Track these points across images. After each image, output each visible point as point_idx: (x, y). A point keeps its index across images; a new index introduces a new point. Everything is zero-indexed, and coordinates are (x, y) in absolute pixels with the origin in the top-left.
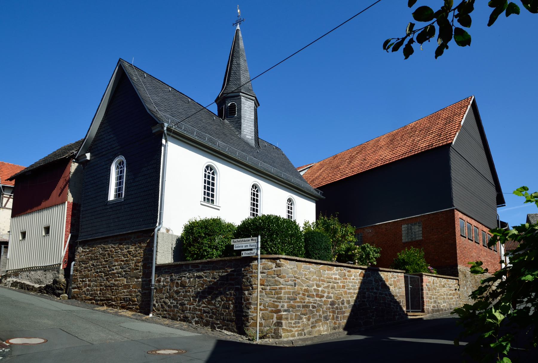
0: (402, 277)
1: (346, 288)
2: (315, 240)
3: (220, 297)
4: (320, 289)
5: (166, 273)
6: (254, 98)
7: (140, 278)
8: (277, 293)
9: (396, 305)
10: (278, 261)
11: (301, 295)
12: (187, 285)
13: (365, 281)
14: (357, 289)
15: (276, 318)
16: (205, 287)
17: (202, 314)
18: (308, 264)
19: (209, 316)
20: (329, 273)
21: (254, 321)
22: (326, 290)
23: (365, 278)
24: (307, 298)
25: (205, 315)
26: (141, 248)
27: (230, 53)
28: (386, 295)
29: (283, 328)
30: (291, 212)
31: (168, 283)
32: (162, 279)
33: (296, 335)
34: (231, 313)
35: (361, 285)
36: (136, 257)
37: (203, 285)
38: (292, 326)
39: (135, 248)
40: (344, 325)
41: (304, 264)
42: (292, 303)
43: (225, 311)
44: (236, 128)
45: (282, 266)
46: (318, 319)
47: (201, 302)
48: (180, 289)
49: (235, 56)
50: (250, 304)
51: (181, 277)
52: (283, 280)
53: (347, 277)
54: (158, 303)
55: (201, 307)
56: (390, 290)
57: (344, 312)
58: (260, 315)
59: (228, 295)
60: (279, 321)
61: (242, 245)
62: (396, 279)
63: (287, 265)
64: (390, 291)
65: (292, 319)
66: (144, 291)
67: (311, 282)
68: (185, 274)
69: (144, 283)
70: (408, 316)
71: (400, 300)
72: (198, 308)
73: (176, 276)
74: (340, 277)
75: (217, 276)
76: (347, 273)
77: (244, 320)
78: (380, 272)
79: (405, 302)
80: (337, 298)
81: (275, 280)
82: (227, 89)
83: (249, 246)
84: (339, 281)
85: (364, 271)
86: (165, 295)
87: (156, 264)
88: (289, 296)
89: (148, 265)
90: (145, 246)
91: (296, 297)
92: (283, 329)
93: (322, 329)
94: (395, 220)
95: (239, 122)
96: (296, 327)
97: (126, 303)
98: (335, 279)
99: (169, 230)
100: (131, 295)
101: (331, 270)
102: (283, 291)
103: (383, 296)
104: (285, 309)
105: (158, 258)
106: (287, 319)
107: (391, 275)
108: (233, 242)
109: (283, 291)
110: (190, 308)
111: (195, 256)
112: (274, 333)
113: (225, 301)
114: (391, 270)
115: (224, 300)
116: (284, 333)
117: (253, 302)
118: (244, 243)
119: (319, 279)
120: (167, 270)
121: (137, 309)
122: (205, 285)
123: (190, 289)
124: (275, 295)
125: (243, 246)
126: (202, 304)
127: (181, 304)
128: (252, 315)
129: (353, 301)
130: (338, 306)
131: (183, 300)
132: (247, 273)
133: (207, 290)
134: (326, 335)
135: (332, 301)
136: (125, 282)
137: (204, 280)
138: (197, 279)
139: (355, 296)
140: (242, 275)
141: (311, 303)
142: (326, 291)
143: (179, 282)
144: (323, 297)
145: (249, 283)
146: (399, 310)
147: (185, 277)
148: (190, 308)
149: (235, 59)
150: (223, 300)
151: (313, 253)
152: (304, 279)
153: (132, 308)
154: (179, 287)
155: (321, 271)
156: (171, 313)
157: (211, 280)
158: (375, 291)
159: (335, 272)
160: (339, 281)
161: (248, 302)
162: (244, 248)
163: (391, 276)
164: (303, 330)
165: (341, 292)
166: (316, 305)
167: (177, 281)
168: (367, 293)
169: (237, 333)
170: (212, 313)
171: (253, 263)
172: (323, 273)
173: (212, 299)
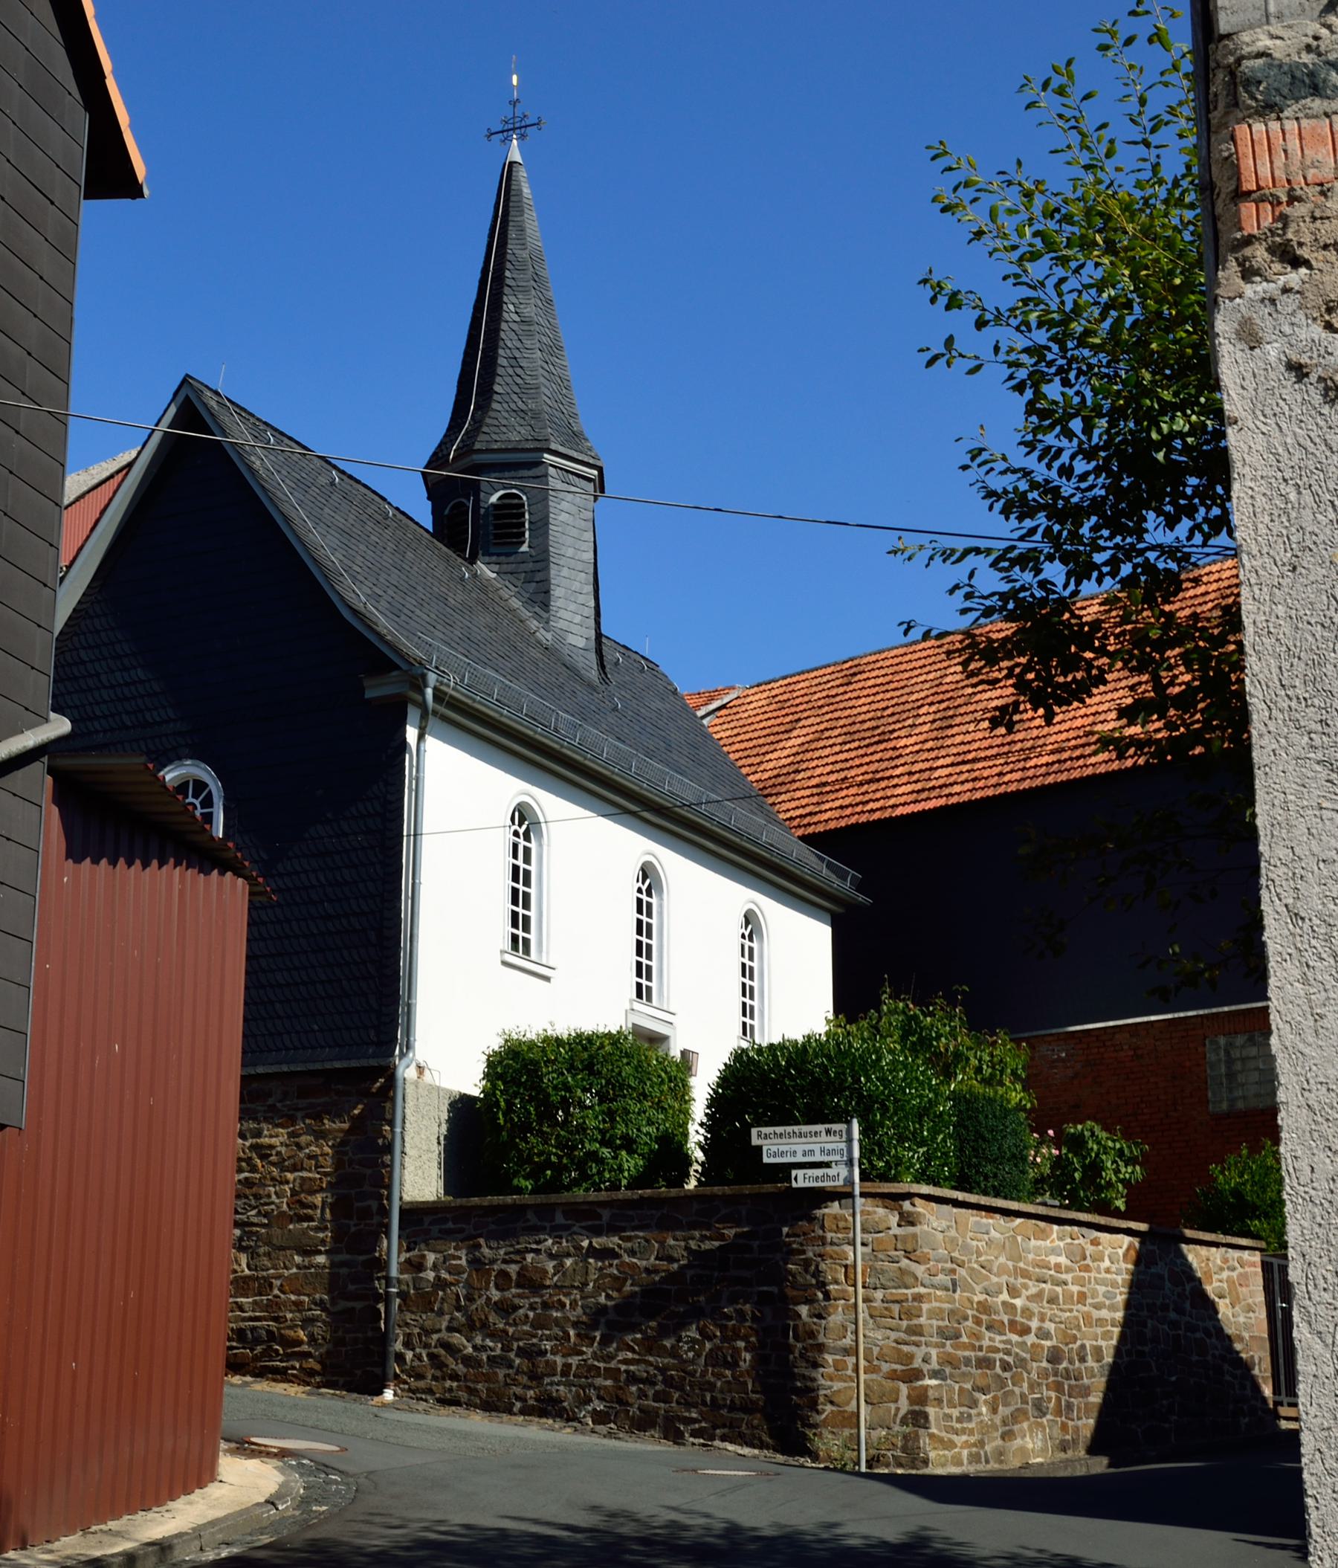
0: (1253, 1265)
1: (1089, 1301)
2: (980, 1123)
3: (694, 1327)
4: (1018, 1302)
5: (447, 1235)
6: (596, 472)
7: (319, 1252)
8: (909, 1314)
9: (1239, 1372)
10: (906, 1205)
11: (969, 1323)
12: (548, 1283)
13: (1141, 1277)
14: (1121, 1306)
15: (909, 1397)
16: (628, 1288)
17: (621, 1388)
18: (984, 1213)
19: (651, 1393)
20: (1039, 1248)
21: (834, 1408)
22: (1034, 1307)
23: (1142, 1267)
24: (988, 1334)
25: (634, 1389)
26: (320, 1135)
27: (480, 265)
28: (1209, 1335)
29: (930, 1431)
31: (459, 1273)
32: (431, 1257)
33: (965, 1461)
34: (745, 1383)
35: (1130, 1293)
36: (294, 1169)
37: (618, 1282)
38: (952, 1427)
39: (291, 1135)
40: (1089, 1435)
42: (951, 1350)
43: (719, 1376)
44: (530, 602)
45: (920, 1223)
46: (1017, 1410)
47: (615, 1345)
48: (519, 1296)
49: (508, 282)
50: (821, 1348)
51: (522, 1253)
52: (922, 1268)
53: (1088, 1261)
54: (413, 1350)
55: (615, 1362)
56: (1220, 1316)
57: (1086, 1391)
59: (729, 1318)
60: (917, 1408)
61: (794, 1147)
62: (1235, 1274)
63: (931, 1218)
64: (1218, 1320)
66: (343, 1304)
67: (994, 1279)
68: (538, 1243)
69: (344, 1271)
70: (1279, 1417)
71: (1252, 1357)
72: (602, 1365)
73: (498, 1248)
74: (1069, 1263)
75: (679, 1252)
76: (1090, 1249)
77: (798, 1406)
78: (1184, 1246)
79: (1267, 1364)
80: (1065, 1338)
81: (900, 1269)
82: (485, 429)
83: (817, 1152)
84: (1068, 1277)
85: (1136, 1241)
86: (447, 1317)
88: (941, 1323)
89: (358, 1204)
90: (341, 1130)
91: (959, 1329)
92: (932, 1436)
93: (1030, 1446)
94: (1176, 1015)
95: (539, 577)
96: (964, 1431)
97: (252, 1350)
98: (1058, 1267)
99: (423, 1068)
100: (276, 1319)
101: (1043, 1235)
102: (925, 1307)
103: (1198, 1335)
105: (408, 1176)
106: (939, 1401)
107: (1218, 1256)
108: (759, 1136)
109: (925, 1307)
110: (567, 1367)
111: (549, 1172)
112: (904, 1449)
113: (717, 1341)
114: (1221, 1238)
115: (715, 1336)
116: (935, 1449)
117: (829, 1342)
118: (798, 1140)
120: (450, 1225)
121: (312, 1373)
122: (629, 1282)
123: (563, 1298)
124: (900, 1319)
125: (795, 1152)
126: (618, 1349)
127: (521, 1352)
128: (830, 1388)
129: (1112, 1351)
130: (1071, 1367)
131: (535, 1336)
132: (802, 1244)
133: (638, 1300)
134: (1042, 1464)
135: (1053, 1347)
136: (244, 1266)
137: (623, 1263)
138: (591, 1261)
139: (1117, 1330)
140: (785, 1249)
141: (997, 1350)
142: (1036, 1311)
143: (513, 1269)
145: (813, 1276)
146: (1248, 1392)
147: (537, 1252)
148: (567, 1367)
149: (513, 299)
150: (706, 1336)
151: (978, 1172)
153: (287, 1368)
154: (513, 1290)
155: (1019, 1238)
156: (480, 1386)
157: (654, 1266)
158: (1173, 1315)
159: (1057, 1243)
160: (1068, 1277)
161: (811, 1342)
162: (800, 1159)
163: (1219, 1262)
164: (981, 1443)
165: (1077, 1318)
166: (1010, 1359)
167: (504, 1266)
168: (1150, 1323)
169: (776, 1450)
170: (664, 1382)
171: (826, 1211)
172: (1024, 1245)
173: (664, 1331)
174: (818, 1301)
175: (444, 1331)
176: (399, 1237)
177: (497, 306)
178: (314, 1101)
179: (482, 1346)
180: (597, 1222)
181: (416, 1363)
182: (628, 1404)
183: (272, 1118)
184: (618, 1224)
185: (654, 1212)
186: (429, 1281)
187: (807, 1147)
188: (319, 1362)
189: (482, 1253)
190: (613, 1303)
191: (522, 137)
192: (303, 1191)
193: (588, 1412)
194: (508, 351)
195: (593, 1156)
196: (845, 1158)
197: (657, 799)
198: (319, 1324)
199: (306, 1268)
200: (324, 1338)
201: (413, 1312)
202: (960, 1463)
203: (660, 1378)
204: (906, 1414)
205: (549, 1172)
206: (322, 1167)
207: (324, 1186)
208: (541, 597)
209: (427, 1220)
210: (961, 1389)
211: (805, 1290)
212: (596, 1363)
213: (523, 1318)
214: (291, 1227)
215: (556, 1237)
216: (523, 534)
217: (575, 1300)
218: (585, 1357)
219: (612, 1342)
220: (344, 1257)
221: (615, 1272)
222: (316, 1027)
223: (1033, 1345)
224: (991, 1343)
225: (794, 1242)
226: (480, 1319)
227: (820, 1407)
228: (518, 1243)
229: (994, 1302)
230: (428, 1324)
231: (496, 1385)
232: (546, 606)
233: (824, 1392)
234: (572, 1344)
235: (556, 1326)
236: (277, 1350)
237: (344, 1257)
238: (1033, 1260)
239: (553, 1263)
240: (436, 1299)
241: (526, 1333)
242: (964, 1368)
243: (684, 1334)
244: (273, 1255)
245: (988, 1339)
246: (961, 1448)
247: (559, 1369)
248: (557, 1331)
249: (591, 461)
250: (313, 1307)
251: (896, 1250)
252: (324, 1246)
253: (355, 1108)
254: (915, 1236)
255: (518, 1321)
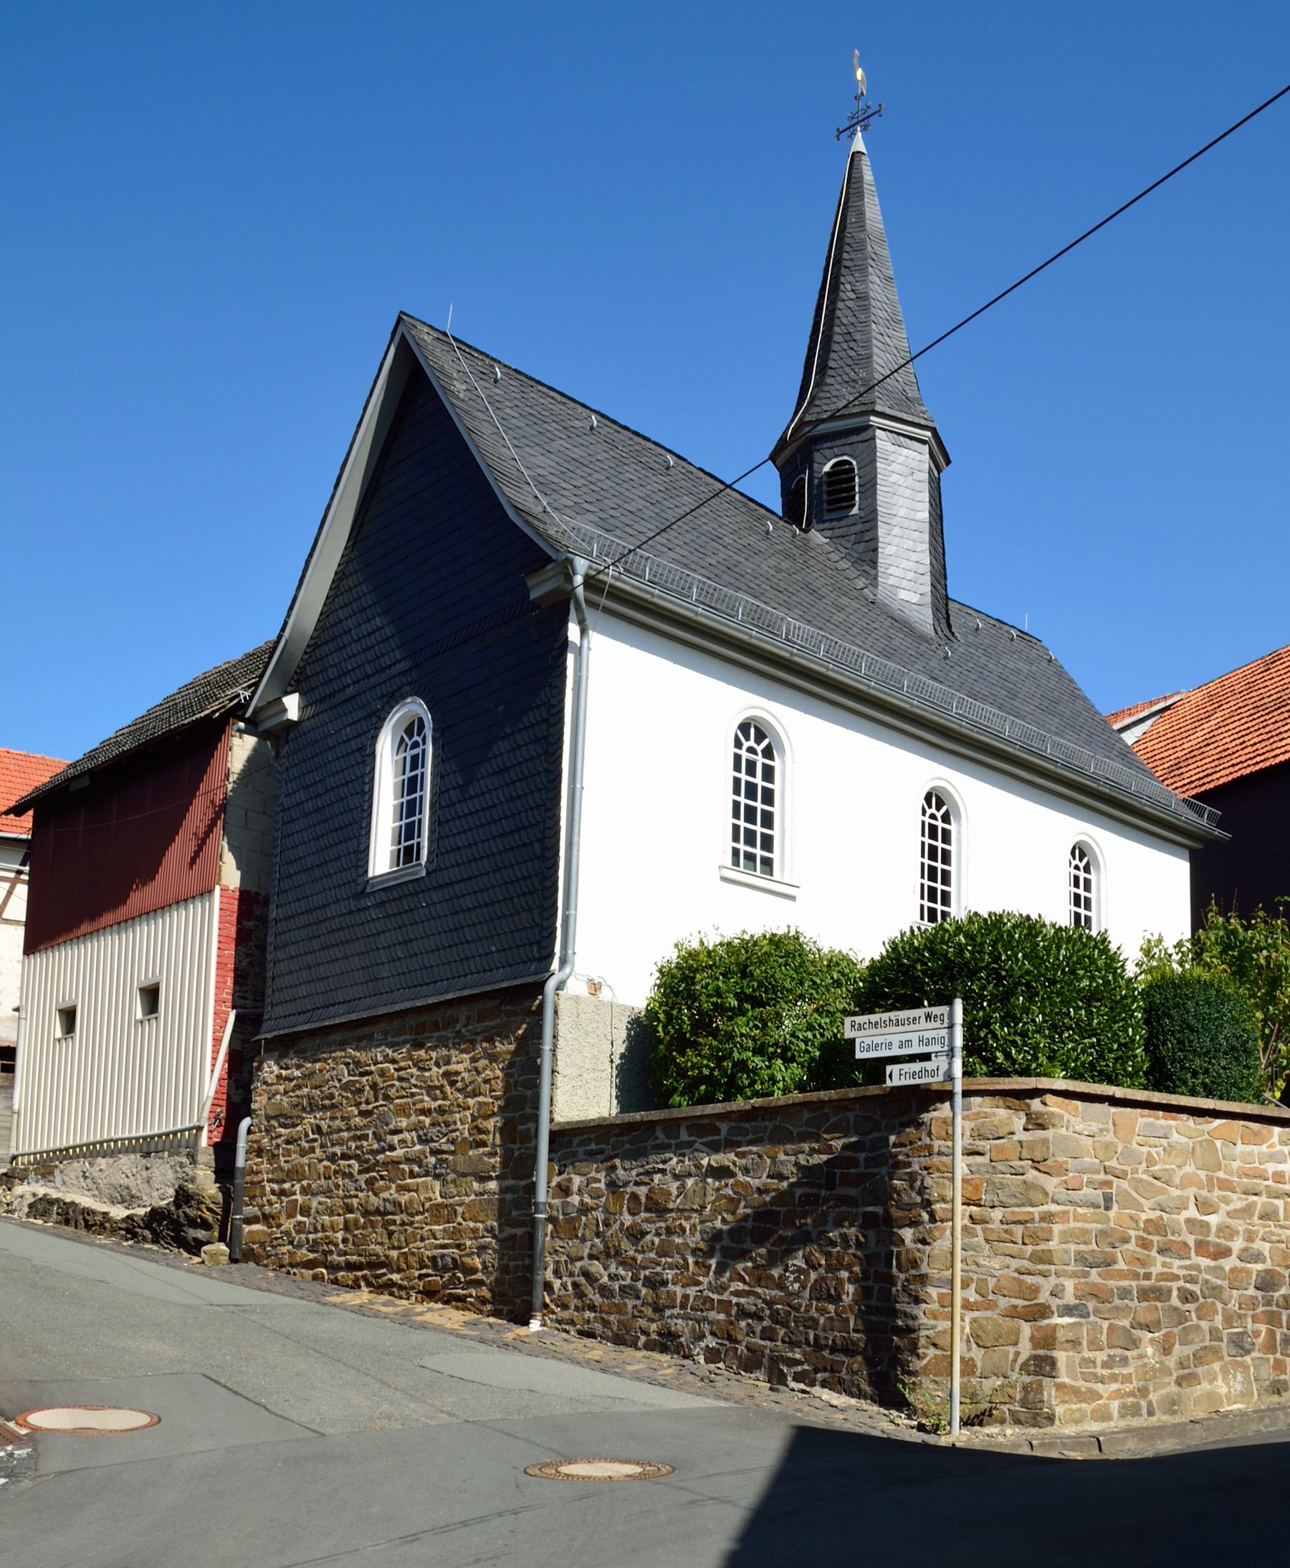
2: (1188, 1012)
3: (801, 1253)
4: (1213, 1220)
5: (591, 1156)
6: (929, 434)
7: (490, 1178)
10: (1035, 1104)
11: (1132, 1246)
12: (671, 1206)
15: (1032, 1339)
16: (741, 1211)
17: (731, 1323)
19: (758, 1329)
21: (938, 1352)
22: (1239, 1225)
24: (1160, 1259)
25: (743, 1324)
26: (493, 1058)
30: (1088, 901)
31: (599, 1197)
32: (577, 1181)
33: (1116, 1415)
34: (847, 1320)
36: (475, 1094)
37: (733, 1202)
38: (1095, 1375)
41: (1142, 1116)
42: (1098, 1280)
43: (822, 1311)
47: (728, 1274)
48: (647, 1220)
50: (923, 1279)
55: (727, 1293)
58: (962, 1329)
59: (833, 1244)
60: (1041, 1352)
61: (889, 1038)
65: (1095, 1345)
66: (510, 1231)
67: (1175, 1192)
68: (664, 1162)
69: (509, 1196)
72: (715, 1297)
75: (789, 1169)
77: (898, 1348)
81: (1025, 1182)
83: (915, 1042)
86: (589, 1244)
87: (552, 1120)
88: (1082, 1247)
90: (508, 1052)
92: (1060, 1387)
93: (1223, 1390)
95: (867, 536)
96: (1114, 1378)
97: (442, 1277)
100: (458, 1246)
101: (1258, 1140)
104: (1065, 1302)
106: (1075, 1344)
109: (1057, 1228)
110: (686, 1297)
112: (1024, 1403)
113: (822, 1271)
115: (820, 1265)
119: (1210, 1179)
120: (593, 1146)
121: (484, 1301)
122: (743, 1204)
124: (1024, 1244)
126: (731, 1280)
127: (649, 1282)
128: (933, 1328)
131: (658, 1264)
132: (908, 1156)
134: (1242, 1414)
135: (1266, 1271)
136: (438, 1194)
138: (709, 1180)
140: (891, 1162)
141: (1177, 1278)
142: (1241, 1229)
143: (642, 1191)
144: (1226, 1252)
147: (663, 1171)
148: (686, 1297)
149: (850, 279)
151: (1182, 1068)
152: (1145, 1177)
153: (466, 1296)
154: (643, 1215)
155: (1218, 1143)
157: (765, 1185)
159: (1278, 1148)
162: (896, 1052)
164: (1143, 1392)
166: (1196, 1288)
169: (874, 1401)
170: (771, 1317)
171: (935, 1114)
173: (773, 1260)
174: (923, 1223)
175: (586, 1259)
176: (550, 1160)
177: (835, 288)
178: (488, 1023)
179: (616, 1275)
180: (716, 1138)
181: (563, 1292)
182: (736, 1341)
183: (459, 1044)
184: (734, 1138)
185: (767, 1123)
186: (574, 1206)
187: (904, 1037)
188: (490, 1290)
189: (616, 1175)
190: (728, 1227)
191: (865, 129)
192: (480, 1117)
193: (702, 1349)
194: (843, 328)
195: (742, 1065)
196: (946, 1048)
197: (936, 718)
198: (490, 1251)
199: (481, 1194)
200: (493, 1266)
201: (561, 1239)
202: (1105, 1416)
203: (768, 1312)
204: (1028, 1360)
205: (703, 1087)
206: (494, 1091)
207: (496, 1110)
208: (868, 557)
209: (576, 1141)
210: (1111, 1327)
211: (910, 1210)
212: (711, 1295)
213: (650, 1244)
214: (471, 1153)
215: (680, 1155)
216: (854, 496)
217: (694, 1225)
218: (701, 1288)
219: (725, 1272)
220: (509, 1182)
221: (731, 1193)
222: (494, 949)
223: (1233, 1270)
224: (1166, 1270)
225: (901, 1152)
226: (614, 1246)
227: (920, 1351)
228: (648, 1163)
229: (1173, 1220)
230: (573, 1252)
231: (625, 1317)
232: (874, 563)
233: (927, 1333)
234: (690, 1273)
235: (678, 1253)
236: (459, 1278)
237: (509, 1182)
238: (1239, 1168)
239: (678, 1184)
240: (580, 1225)
241: (652, 1261)
242: (1117, 1302)
243: (790, 1262)
244: (458, 1182)
245: (1158, 1265)
246: (1109, 1398)
247: (678, 1301)
248: (678, 1259)
249: (923, 422)
250: (485, 1233)
251: (1020, 1159)
252: (495, 1171)
253: (519, 1028)
254: (1045, 1142)
255: (645, 1248)
